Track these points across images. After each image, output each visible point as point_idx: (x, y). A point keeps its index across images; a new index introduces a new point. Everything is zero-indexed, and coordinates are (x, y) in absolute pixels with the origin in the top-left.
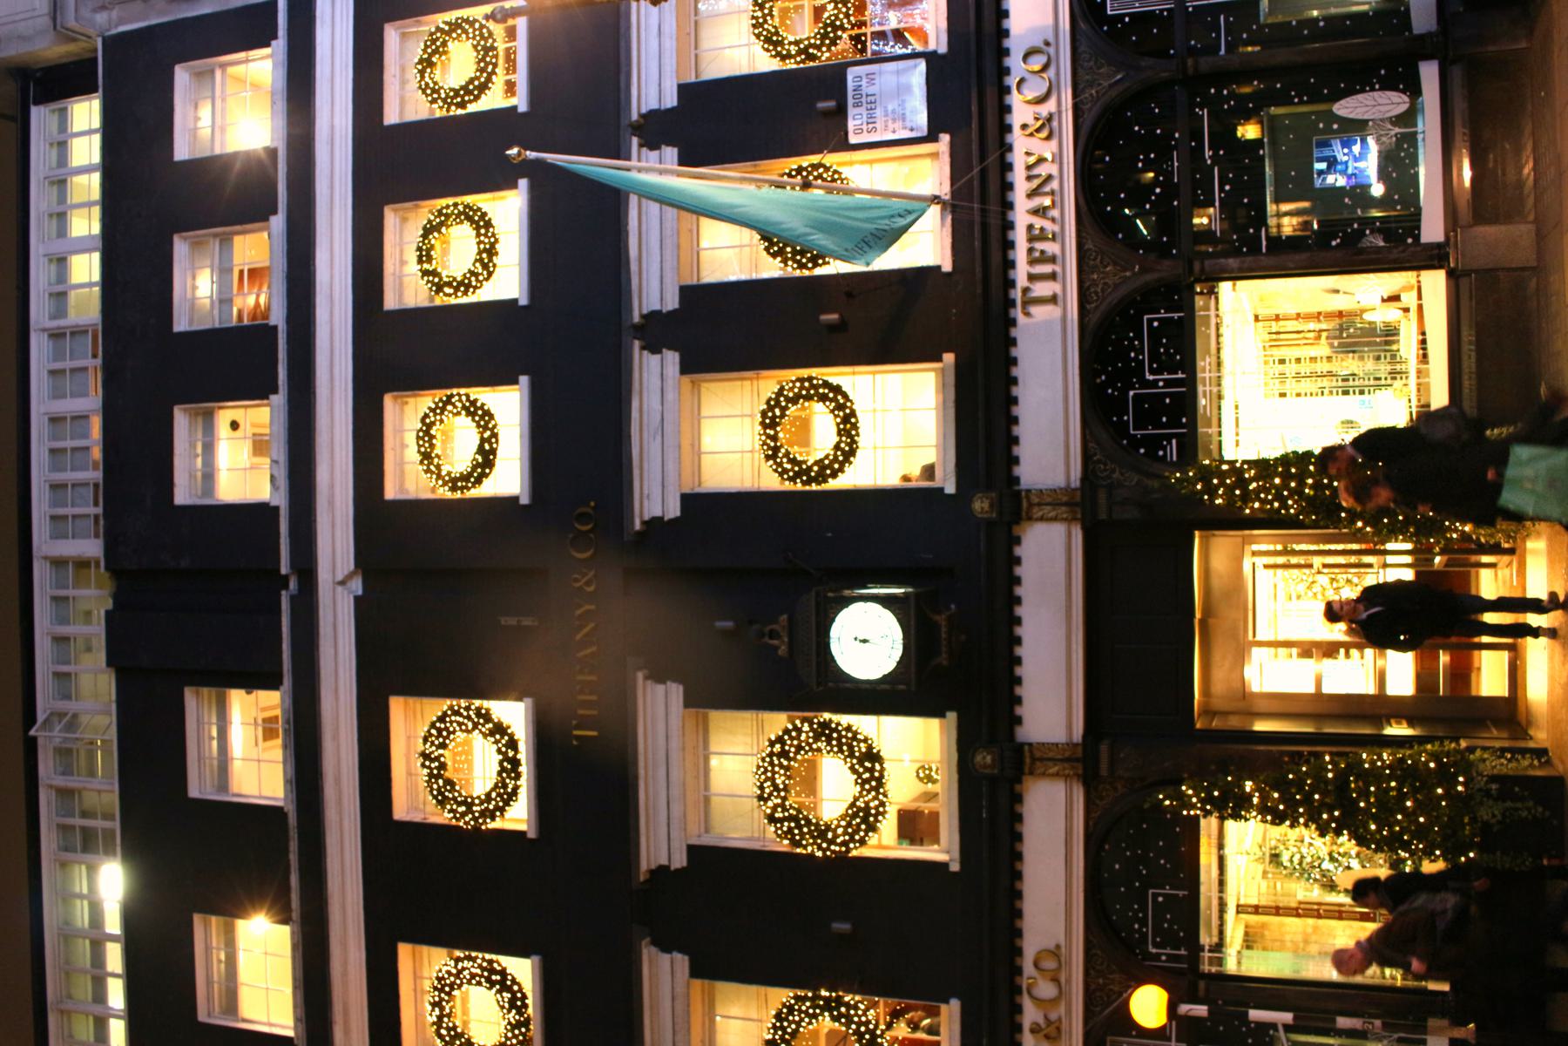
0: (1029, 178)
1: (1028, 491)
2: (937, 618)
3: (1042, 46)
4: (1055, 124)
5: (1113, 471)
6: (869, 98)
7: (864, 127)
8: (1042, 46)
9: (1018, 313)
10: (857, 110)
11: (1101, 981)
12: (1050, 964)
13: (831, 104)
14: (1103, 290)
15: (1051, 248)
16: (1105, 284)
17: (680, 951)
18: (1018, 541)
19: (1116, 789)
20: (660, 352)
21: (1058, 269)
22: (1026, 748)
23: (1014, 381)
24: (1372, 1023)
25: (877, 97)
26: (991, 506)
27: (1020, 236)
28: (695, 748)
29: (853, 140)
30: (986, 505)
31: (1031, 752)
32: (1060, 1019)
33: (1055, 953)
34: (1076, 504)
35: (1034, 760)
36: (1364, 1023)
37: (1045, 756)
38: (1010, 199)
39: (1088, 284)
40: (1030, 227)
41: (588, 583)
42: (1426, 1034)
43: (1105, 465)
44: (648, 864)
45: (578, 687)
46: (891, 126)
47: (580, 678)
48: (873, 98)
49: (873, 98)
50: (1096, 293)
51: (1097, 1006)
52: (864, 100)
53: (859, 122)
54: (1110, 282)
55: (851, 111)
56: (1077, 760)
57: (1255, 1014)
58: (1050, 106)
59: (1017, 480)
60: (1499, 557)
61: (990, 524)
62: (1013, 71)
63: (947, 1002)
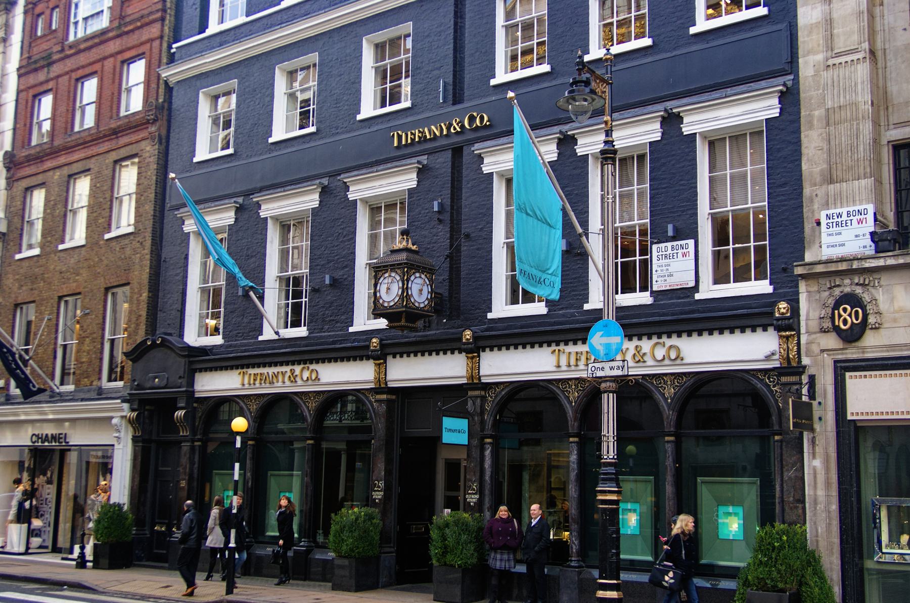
2: (403, 320)
5: (491, 397)
6: (675, 255)
7: (661, 253)
10: (670, 248)
12: (673, 356)
13: (670, 233)
14: (567, 391)
20: (661, 128)
21: (573, 368)
25: (676, 259)
32: (644, 362)
33: (317, 378)
38: (736, 331)
46: (659, 269)
47: (409, 133)
48: (849, 224)
50: (566, 387)
52: (675, 251)
53: (663, 250)
55: (669, 245)
57: (237, 465)
58: (650, 362)
59: (484, 351)
63: (771, 284)
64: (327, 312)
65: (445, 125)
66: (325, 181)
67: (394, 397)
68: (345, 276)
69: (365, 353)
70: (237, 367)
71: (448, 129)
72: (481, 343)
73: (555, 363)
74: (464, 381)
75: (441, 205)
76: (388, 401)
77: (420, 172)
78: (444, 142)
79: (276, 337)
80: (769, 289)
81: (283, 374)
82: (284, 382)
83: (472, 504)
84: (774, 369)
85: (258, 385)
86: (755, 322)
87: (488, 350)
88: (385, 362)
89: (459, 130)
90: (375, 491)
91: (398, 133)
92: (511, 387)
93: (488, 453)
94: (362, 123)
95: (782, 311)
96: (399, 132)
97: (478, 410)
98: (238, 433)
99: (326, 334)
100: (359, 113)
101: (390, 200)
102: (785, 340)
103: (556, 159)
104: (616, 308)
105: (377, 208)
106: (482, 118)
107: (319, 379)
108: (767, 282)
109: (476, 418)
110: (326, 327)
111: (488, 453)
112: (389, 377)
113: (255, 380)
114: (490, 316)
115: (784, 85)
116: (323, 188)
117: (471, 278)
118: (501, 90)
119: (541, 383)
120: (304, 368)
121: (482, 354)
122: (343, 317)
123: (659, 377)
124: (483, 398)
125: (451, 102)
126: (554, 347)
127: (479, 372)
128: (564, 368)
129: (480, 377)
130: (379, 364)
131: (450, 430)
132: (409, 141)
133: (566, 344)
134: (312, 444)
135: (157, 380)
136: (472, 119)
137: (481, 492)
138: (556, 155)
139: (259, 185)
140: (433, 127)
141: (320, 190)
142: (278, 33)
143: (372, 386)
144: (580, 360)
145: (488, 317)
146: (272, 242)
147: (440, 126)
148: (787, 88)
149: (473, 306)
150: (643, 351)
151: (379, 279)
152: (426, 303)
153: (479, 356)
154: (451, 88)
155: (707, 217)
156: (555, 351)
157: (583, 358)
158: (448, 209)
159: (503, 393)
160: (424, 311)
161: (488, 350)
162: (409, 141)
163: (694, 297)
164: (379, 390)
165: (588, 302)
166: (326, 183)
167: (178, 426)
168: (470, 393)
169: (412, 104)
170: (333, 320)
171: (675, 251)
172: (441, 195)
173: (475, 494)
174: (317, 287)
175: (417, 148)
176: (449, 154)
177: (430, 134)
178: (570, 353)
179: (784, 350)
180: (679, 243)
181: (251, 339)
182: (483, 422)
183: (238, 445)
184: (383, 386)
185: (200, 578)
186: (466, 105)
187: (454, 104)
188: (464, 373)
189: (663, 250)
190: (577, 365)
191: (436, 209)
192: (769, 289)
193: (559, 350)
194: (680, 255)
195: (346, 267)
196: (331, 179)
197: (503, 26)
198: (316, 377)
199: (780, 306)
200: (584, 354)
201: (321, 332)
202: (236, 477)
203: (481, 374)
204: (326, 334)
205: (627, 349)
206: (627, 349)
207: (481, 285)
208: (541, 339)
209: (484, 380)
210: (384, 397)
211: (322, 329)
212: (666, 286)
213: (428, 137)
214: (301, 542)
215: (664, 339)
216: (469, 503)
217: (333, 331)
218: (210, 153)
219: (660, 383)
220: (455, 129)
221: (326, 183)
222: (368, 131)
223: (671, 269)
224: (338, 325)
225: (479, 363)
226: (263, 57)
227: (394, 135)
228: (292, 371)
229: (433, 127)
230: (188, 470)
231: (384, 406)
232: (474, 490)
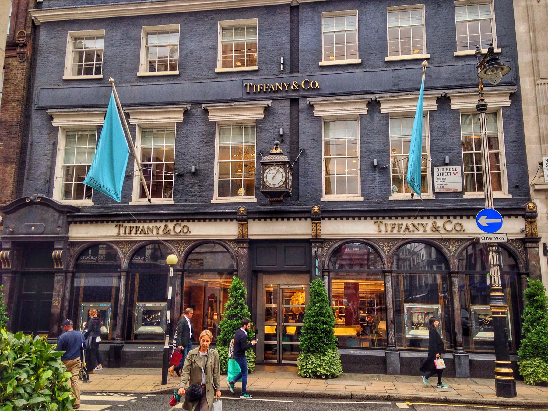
0: (418, 224)
1: (320, 223)
3: (463, 229)
4: (437, 232)
7: (439, 172)
8: (463, 229)
15: (133, 233)
16: (384, 246)
19: (235, 248)
22: (246, 222)
23: (277, 220)
27: (399, 221)
28: (541, 109)
29: (435, 168)
31: (245, 224)
35: (243, 225)
40: (139, 227)
41: (294, 87)
42: (401, 333)
46: (439, 180)
49: (449, 174)
52: (449, 171)
53: (441, 170)
55: (445, 167)
58: (442, 231)
62: (384, 220)
63: (92, 202)
66: (189, 107)
69: (308, 215)
70: (113, 222)
71: (289, 86)
74: (310, 237)
82: (158, 233)
84: (236, 240)
86: (443, 214)
88: (247, 223)
91: (250, 85)
95: (316, 210)
98: (172, 266)
102: (529, 223)
104: (493, 199)
107: (190, 232)
113: (130, 231)
117: (307, 176)
118: (240, 74)
120: (175, 225)
126: (375, 220)
135: (33, 228)
142: (65, 11)
145: (321, 200)
146: (138, 141)
149: (308, 193)
151: (266, 170)
167: (54, 262)
171: (449, 171)
178: (126, 227)
179: (530, 229)
180: (451, 167)
185: (443, 379)
187: (291, 73)
188: (310, 232)
189: (441, 170)
190: (130, 234)
192: (255, 200)
194: (452, 174)
199: (315, 208)
201: (185, 202)
205: (160, 226)
207: (314, 181)
212: (443, 190)
218: (222, 67)
220: (294, 87)
223: (446, 181)
226: (229, 11)
228: (166, 226)
230: (61, 294)
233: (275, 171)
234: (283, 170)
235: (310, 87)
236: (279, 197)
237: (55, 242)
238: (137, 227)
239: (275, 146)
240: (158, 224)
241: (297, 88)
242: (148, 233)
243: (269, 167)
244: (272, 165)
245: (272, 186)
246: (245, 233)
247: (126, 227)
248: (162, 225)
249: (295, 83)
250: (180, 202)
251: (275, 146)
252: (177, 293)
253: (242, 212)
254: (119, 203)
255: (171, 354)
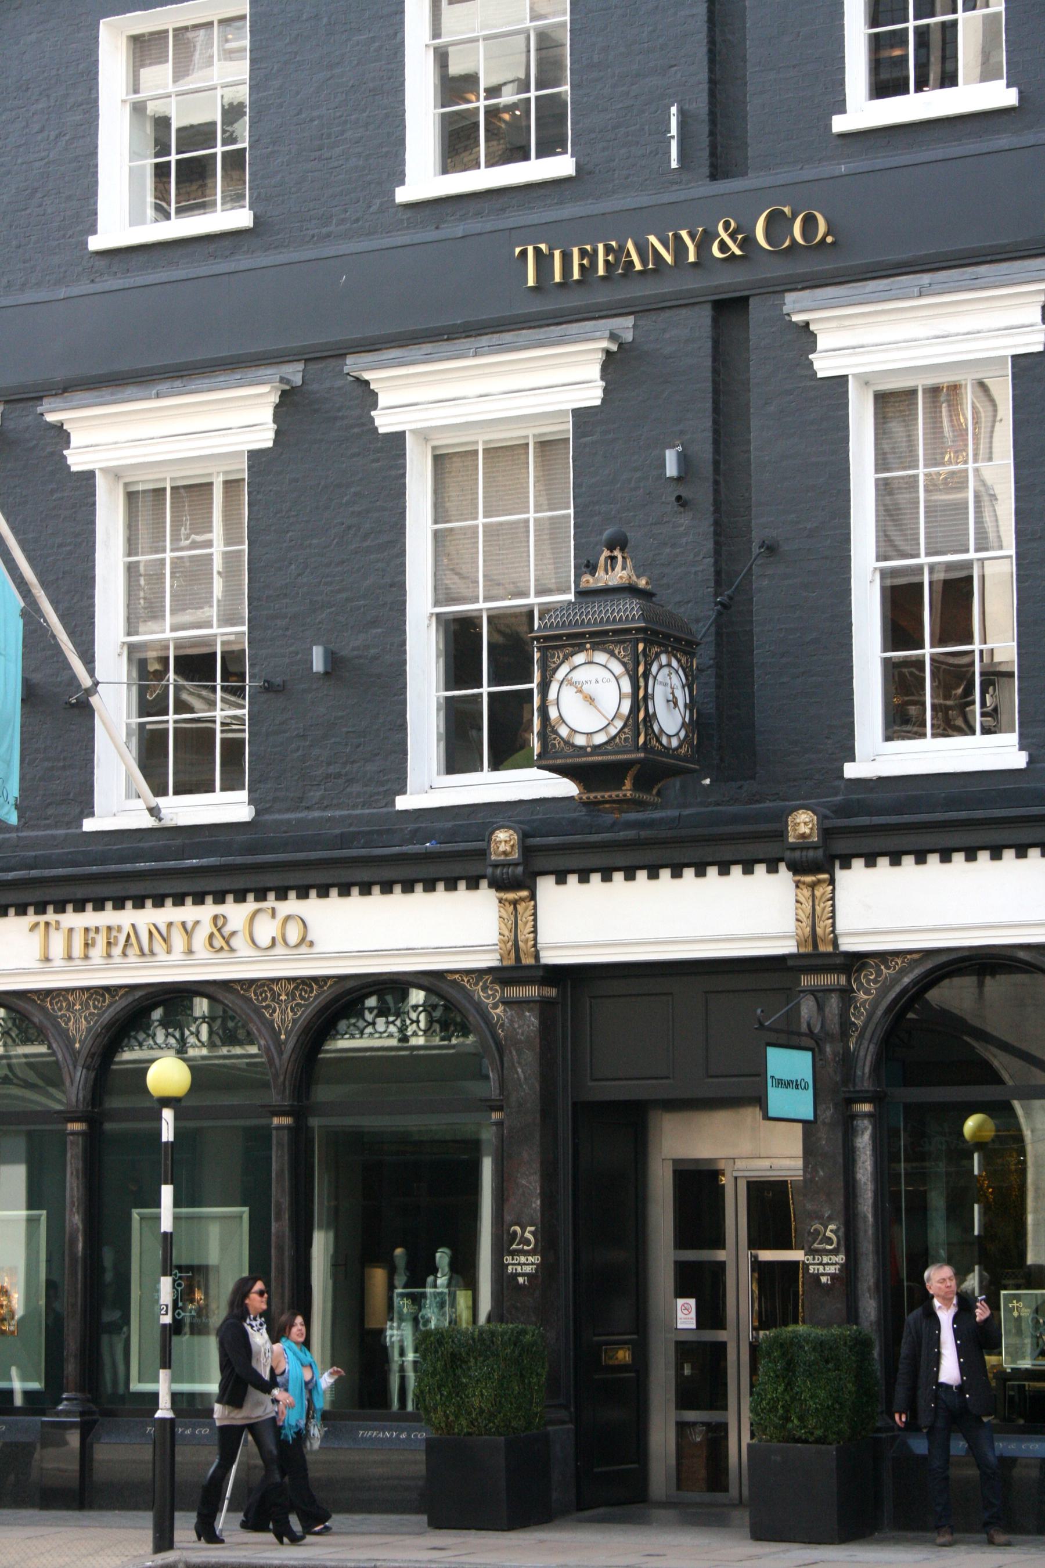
5: (867, 992)
9: (31, 918)
11: (283, 997)
15: (97, 952)
17: (605, 390)
18: (772, 869)
24: (167, 1314)
26: (803, 836)
30: (804, 829)
34: (815, 945)
36: (167, 1306)
37: (817, 903)
39: (71, 998)
40: (119, 929)
41: (723, 246)
43: (875, 981)
44: (816, 320)
45: (588, 247)
47: (576, 251)
51: (51, 1004)
54: (276, 1015)
56: (518, 958)
57: (167, 1192)
59: (846, 865)
60: (253, 1443)
61: (781, 834)
64: (316, 751)
65: (692, 236)
67: (553, 992)
68: (373, 651)
71: (703, 247)
72: (841, 846)
73: (37, 952)
75: (684, 460)
76: (544, 1006)
77: (611, 363)
78: (692, 283)
79: (148, 822)
80: (1019, 760)
81: (188, 931)
82: (190, 951)
83: (824, 1279)
84: (490, 970)
85: (117, 959)
86: (80, 892)
87: (858, 864)
88: (533, 897)
89: (738, 252)
90: (513, 1253)
91: (538, 251)
92: (929, 965)
93: (864, 1141)
94: (409, 214)
96: (543, 247)
97: (834, 1026)
98: (166, 1102)
99: (316, 814)
100: (402, 182)
101: (193, 475)
103: (598, 402)
105: (155, 490)
106: (810, 222)
108: (1012, 738)
109: (828, 1049)
110: (316, 794)
111: (864, 1141)
112: (544, 937)
114: (851, 771)
115: (613, 337)
116: (284, 394)
119: (1021, 955)
121: (840, 875)
122: (371, 768)
123: (58, 995)
124: (846, 994)
125: (706, 171)
127: (833, 925)
128: (58, 962)
129: (836, 938)
130: (515, 903)
131: (796, 1085)
132: (576, 275)
133: (60, 909)
134: (288, 1127)
136: (777, 223)
137: (850, 1244)
138: (271, 435)
139: (60, 375)
140: (653, 239)
141: (275, 398)
143: (489, 960)
144: (94, 944)
147: (678, 238)
148: (620, 345)
150: (227, 930)
152: (682, 734)
153: (832, 882)
154: (704, 129)
155: (426, 622)
156: (37, 925)
157: (101, 940)
158: (708, 471)
159: (906, 980)
160: (678, 758)
161: (858, 864)
162: (576, 275)
163: (393, 803)
164: (515, 974)
165: (92, 814)
166: (298, 380)
168: (807, 981)
169: (579, 167)
170: (338, 776)
172: (682, 432)
173: (835, 1252)
174: (278, 680)
175: (602, 296)
176: (704, 316)
177: (644, 261)
178: (71, 930)
181: (56, 826)
182: (847, 1061)
183: (167, 1134)
184: (529, 961)
186: (752, 181)
187: (713, 177)
191: (671, 469)
193: (47, 924)
195: (374, 623)
196: (314, 367)
197: (124, 101)
198: (303, 939)
200: (103, 933)
202: (166, 1224)
203: (840, 927)
204: (316, 814)
205: (197, 923)
206: (197, 923)
208: (80, 892)
209: (848, 945)
210: (532, 991)
211: (301, 799)
213: (638, 267)
214: (60, 1401)
215: (271, 901)
216: (817, 1277)
217: (338, 806)
219: (60, 1009)
220: (723, 246)
221: (298, 380)
222: (431, 235)
224: (355, 788)
225: (833, 899)
227: (524, 253)
229: (653, 239)
231: (532, 1020)
232: (829, 1241)
233: (567, 693)
234: (624, 664)
235: (793, 240)
236: (619, 785)
237: (751, 301)
238: (109, 929)
239: (606, 553)
240: (189, 912)
241: (738, 252)
242: (152, 953)
243: (566, 658)
244: (580, 648)
245: (580, 741)
246: (526, 941)
247: (71, 930)
248: (207, 911)
249: (726, 228)
250: (280, 811)
251: (606, 553)
252: (279, 1204)
253: (502, 847)
254: (16, 829)
255: (194, 1429)
